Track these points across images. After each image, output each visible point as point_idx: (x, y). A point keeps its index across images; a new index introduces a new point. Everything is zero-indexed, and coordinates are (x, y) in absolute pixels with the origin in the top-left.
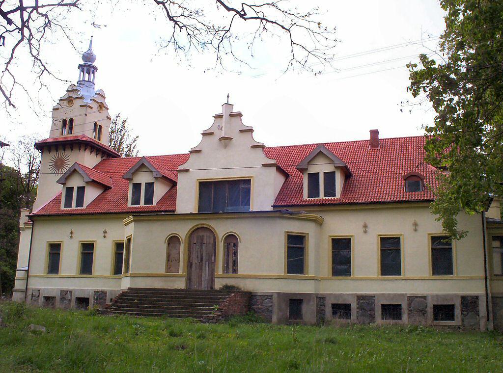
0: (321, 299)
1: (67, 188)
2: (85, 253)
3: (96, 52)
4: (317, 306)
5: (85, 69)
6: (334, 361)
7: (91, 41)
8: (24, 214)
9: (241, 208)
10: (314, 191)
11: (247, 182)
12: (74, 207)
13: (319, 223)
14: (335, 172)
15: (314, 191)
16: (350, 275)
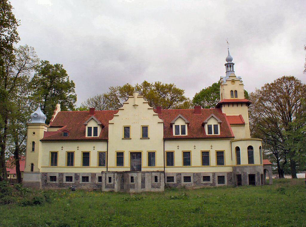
1: (88, 127)
3: (232, 56)
5: (229, 65)
7: (228, 51)
14: (217, 125)
15: (90, 134)
16: (190, 165)
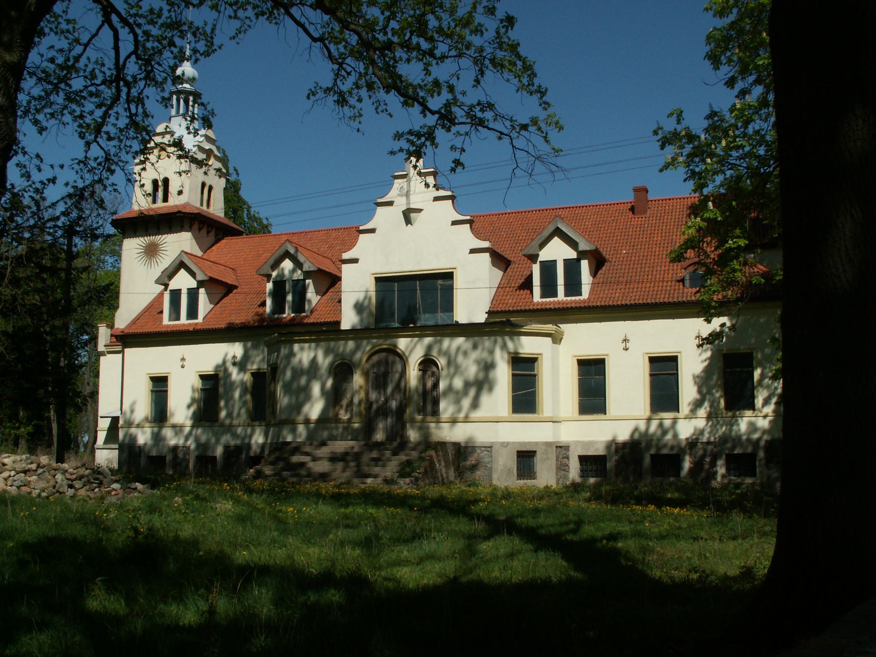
0: (562, 449)
2: (156, 391)
4: (557, 460)
6: (22, 511)
8: (104, 334)
9: (440, 318)
10: (549, 288)
11: (448, 276)
12: (184, 320)
13: (557, 338)
15: (549, 288)
